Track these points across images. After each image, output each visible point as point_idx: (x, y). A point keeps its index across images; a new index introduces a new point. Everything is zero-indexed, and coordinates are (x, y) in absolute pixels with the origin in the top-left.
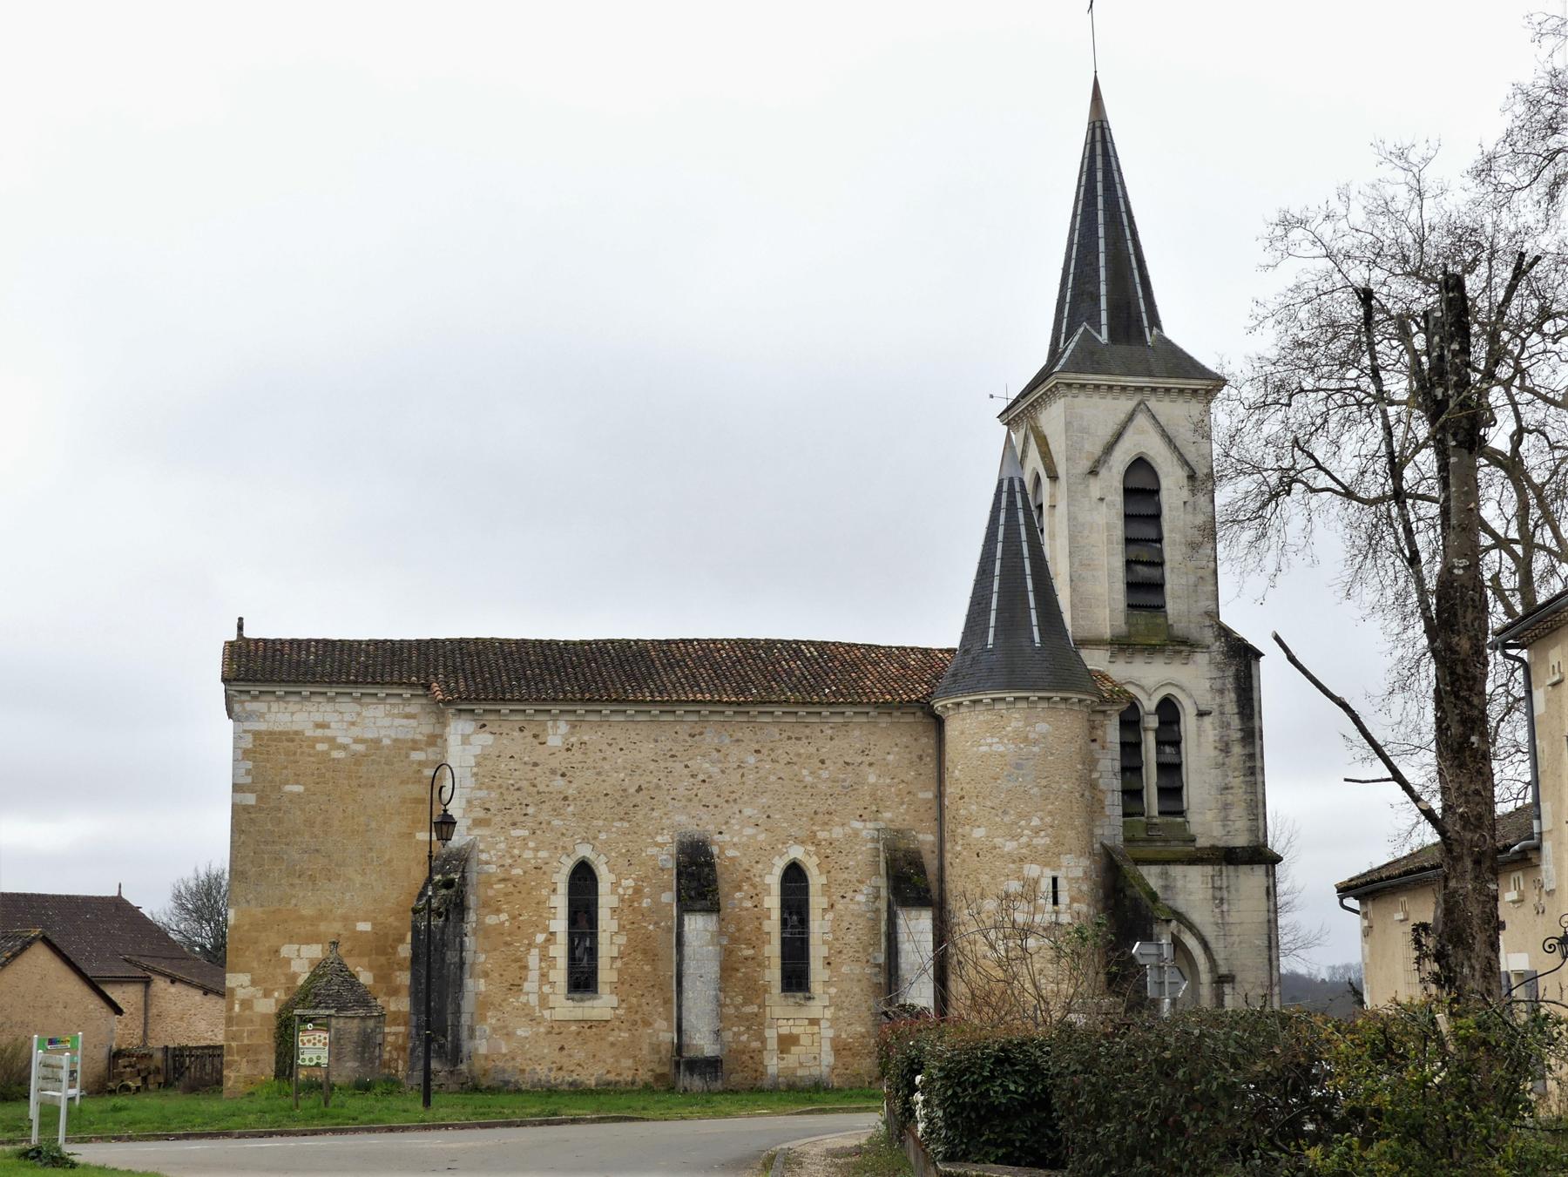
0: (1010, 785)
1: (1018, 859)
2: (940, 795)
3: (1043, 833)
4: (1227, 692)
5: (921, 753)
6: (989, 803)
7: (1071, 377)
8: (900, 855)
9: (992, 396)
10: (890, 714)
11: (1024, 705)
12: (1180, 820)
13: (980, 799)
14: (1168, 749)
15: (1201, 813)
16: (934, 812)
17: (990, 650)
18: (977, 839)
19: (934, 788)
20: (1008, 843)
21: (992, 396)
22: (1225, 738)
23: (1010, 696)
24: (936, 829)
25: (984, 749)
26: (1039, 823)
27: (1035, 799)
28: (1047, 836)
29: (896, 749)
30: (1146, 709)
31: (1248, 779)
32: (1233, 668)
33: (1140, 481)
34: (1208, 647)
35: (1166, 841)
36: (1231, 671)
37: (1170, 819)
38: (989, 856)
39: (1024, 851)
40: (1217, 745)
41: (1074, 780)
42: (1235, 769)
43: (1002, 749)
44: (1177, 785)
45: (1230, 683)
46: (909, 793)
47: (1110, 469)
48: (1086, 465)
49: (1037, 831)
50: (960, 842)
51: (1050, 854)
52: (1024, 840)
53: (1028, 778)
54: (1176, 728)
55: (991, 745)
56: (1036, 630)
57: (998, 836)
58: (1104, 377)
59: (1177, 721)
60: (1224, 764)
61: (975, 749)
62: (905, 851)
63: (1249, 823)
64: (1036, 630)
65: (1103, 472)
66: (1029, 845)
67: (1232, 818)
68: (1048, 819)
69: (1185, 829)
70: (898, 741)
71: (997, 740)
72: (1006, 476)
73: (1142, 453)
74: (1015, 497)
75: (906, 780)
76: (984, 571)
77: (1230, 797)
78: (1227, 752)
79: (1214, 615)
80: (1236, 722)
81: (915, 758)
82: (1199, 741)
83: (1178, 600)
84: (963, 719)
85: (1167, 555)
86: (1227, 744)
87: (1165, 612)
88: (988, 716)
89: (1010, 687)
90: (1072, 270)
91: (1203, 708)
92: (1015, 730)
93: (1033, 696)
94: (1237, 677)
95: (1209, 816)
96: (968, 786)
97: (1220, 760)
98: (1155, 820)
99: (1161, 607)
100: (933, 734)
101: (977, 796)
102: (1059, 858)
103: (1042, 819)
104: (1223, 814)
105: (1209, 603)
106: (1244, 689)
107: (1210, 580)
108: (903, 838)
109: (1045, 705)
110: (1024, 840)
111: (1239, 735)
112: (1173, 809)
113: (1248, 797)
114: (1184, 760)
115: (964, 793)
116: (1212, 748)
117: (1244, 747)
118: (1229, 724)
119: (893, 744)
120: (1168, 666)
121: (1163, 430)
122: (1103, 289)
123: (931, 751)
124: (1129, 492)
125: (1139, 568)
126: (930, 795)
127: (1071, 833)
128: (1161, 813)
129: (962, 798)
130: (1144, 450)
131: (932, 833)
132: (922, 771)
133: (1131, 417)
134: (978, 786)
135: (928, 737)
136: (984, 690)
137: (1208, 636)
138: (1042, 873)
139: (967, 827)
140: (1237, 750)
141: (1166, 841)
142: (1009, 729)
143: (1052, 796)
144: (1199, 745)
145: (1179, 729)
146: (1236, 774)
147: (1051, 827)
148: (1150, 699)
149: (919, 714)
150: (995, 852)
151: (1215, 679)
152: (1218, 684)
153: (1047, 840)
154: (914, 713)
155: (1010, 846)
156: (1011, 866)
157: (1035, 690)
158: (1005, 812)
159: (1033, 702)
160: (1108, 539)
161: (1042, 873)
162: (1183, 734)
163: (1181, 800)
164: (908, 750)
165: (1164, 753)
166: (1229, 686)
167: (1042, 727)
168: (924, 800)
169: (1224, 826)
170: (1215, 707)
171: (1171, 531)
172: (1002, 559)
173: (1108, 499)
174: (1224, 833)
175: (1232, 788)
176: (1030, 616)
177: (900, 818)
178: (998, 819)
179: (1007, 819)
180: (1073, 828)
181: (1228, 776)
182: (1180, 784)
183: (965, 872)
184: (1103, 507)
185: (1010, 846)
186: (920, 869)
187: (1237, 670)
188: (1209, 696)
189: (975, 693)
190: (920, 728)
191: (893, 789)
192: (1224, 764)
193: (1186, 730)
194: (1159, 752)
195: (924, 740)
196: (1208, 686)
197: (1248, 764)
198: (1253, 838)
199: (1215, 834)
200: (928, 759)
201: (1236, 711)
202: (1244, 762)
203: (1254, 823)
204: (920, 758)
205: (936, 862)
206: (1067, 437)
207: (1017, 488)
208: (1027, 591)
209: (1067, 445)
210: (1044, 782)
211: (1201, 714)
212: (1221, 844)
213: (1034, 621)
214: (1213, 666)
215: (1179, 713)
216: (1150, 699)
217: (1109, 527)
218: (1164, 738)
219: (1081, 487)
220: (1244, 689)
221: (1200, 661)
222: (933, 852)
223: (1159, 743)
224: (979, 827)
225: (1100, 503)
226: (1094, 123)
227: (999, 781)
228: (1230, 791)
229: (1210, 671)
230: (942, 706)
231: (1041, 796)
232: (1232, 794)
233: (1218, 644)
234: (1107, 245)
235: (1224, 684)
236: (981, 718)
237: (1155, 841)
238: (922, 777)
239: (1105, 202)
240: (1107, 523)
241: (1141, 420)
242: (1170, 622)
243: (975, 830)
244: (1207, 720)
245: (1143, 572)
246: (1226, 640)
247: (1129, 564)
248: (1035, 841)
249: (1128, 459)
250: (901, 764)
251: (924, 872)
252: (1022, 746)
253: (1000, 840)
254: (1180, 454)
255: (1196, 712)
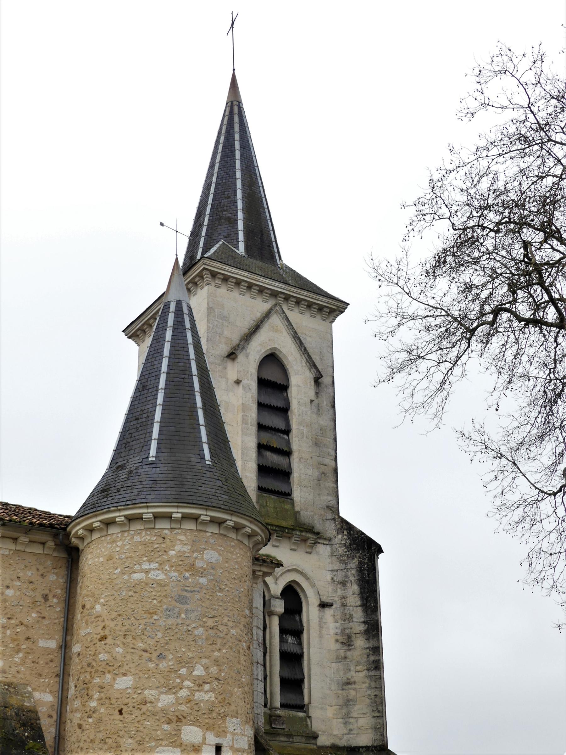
0: (170, 621)
1: (175, 719)
2: (65, 646)
3: (207, 687)
4: (349, 585)
5: (47, 592)
6: (141, 645)
7: (216, 266)
8: (10, 713)
9: (162, 224)
10: (15, 540)
11: (191, 526)
12: (301, 714)
13: (129, 639)
14: (290, 639)
15: (322, 708)
16: (56, 667)
17: (152, 463)
18: (121, 691)
19: (59, 636)
20: (163, 697)
21: (162, 224)
22: (347, 631)
23: (177, 512)
24: (56, 687)
25: (136, 576)
26: (204, 673)
27: (200, 642)
28: (212, 690)
29: (18, 583)
30: (273, 593)
31: (372, 673)
32: (356, 561)
33: (272, 375)
34: (330, 540)
35: (289, 736)
36: (354, 564)
37: (292, 713)
38: (137, 713)
39: (183, 708)
40: (339, 638)
41: (241, 626)
42: (358, 663)
43: (162, 576)
44: (299, 677)
45: (353, 575)
46: (28, 638)
47: (247, 356)
48: (225, 349)
49: (200, 683)
50: (96, 696)
51: (214, 715)
52: (183, 693)
53: (193, 615)
54: (298, 618)
55: (147, 572)
56: (206, 448)
57: (151, 688)
58: (246, 274)
59: (299, 611)
60: (345, 658)
61: (126, 577)
62: (18, 709)
63: (373, 720)
64: (206, 448)
65: (241, 357)
66: (189, 701)
67: (354, 715)
68: (214, 670)
69: (307, 725)
70: (21, 575)
71: (156, 565)
72: (172, 298)
73: (275, 348)
74: (183, 318)
75: (25, 621)
76: (144, 387)
77: (353, 693)
78: (349, 645)
79: (335, 510)
80: (359, 614)
81: (40, 599)
82: (320, 632)
83: (305, 489)
84: (114, 542)
85: (295, 446)
86: (349, 637)
87: (292, 500)
88: (147, 537)
89: (180, 501)
90: (210, 201)
91: (325, 599)
92: (180, 555)
93: (205, 515)
94: (360, 570)
95: (330, 712)
96: (112, 624)
97: (342, 653)
98: (278, 712)
99: (288, 495)
100: (63, 572)
101: (125, 636)
102: (224, 721)
103: (206, 668)
104: (344, 711)
105: (330, 498)
106: (368, 582)
107: (331, 475)
108: (17, 693)
109: (214, 529)
110: (183, 693)
111: (362, 628)
112: (293, 702)
113: (372, 692)
114: (305, 651)
115: (107, 632)
116: (333, 640)
117: (368, 640)
118: (351, 617)
119: (15, 577)
120: (292, 552)
121: (295, 332)
122: (240, 215)
123: (59, 591)
124: (262, 383)
125: (268, 454)
126: (53, 644)
127: (238, 691)
128: (283, 706)
129: (103, 638)
130: (276, 346)
131: (51, 692)
132: (45, 614)
133: (267, 315)
134: (127, 622)
135: (56, 574)
136: (146, 504)
137: (330, 529)
138: (204, 739)
139: (108, 676)
140: (360, 643)
141: (289, 736)
142: (172, 553)
143: (219, 641)
144: (321, 636)
145: (301, 619)
146: (358, 668)
147: (217, 679)
148: (276, 583)
149: (51, 544)
150: (144, 708)
151: (337, 571)
152: (340, 576)
153: (211, 696)
154: (43, 544)
155: (166, 700)
156: (166, 727)
157: (208, 507)
158: (161, 656)
159: (148, 521)
160: (243, 419)
161: (204, 739)
162: (305, 624)
163: (301, 693)
164: (31, 586)
165: (287, 642)
166: (352, 578)
167: (211, 555)
168: (46, 649)
169: (345, 723)
170: (336, 599)
171: (300, 424)
172: (168, 373)
173: (244, 382)
174: (345, 731)
175: (355, 683)
176: (200, 433)
177: (14, 670)
178: (151, 665)
179: (163, 665)
180: (241, 686)
181: (350, 670)
182: (301, 677)
183: (100, 736)
184: (240, 390)
185: (166, 700)
186: (38, 734)
187: (360, 563)
188: (330, 588)
189: (134, 505)
190: (49, 563)
191: (8, 632)
192: (345, 658)
193: (308, 621)
194: (282, 640)
195: (53, 577)
196: (329, 577)
197: (372, 658)
198: (378, 737)
199: (335, 733)
200: (55, 600)
201: (359, 603)
202: (368, 656)
203: (380, 720)
204: (46, 597)
205: (53, 730)
206: (208, 320)
207: (185, 310)
208: (196, 407)
209: (208, 327)
210: (210, 623)
211: (323, 605)
212: (342, 743)
213: (204, 438)
214: (334, 558)
215: (301, 603)
216: (276, 583)
217: (244, 407)
218: (287, 626)
219: (219, 368)
220: (368, 582)
221: (321, 552)
222: (50, 716)
223: (283, 631)
224: (125, 675)
225: (235, 385)
226: (232, 103)
227: (156, 617)
228: (353, 686)
229: (332, 563)
230: (83, 528)
231: (207, 639)
232: (355, 689)
233: (340, 536)
234: (243, 185)
235: (346, 576)
236: (137, 539)
237: (279, 734)
238: (46, 622)
239: (242, 155)
240: (243, 404)
241: (275, 320)
242: (297, 509)
243: (118, 680)
244: (329, 612)
245: (273, 459)
246: (349, 533)
247: (261, 447)
248: (198, 696)
249: (263, 351)
250: (22, 603)
251: (42, 737)
252: (187, 575)
253: (152, 692)
254: (309, 356)
255: (318, 603)
